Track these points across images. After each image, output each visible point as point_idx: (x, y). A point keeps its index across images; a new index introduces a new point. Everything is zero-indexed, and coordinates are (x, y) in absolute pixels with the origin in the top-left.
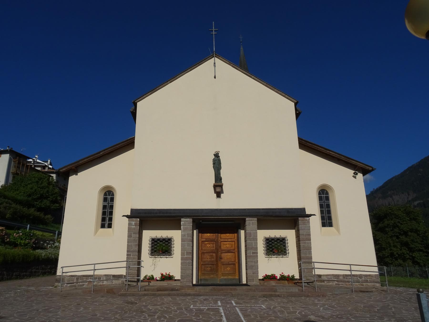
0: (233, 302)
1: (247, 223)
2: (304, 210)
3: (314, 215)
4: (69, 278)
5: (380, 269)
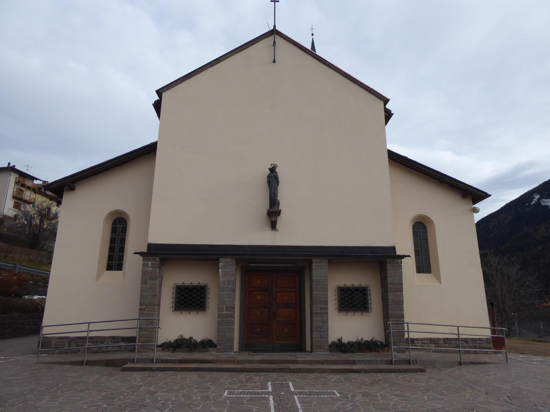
0: (291, 384)
1: (314, 266)
2: (393, 249)
3: (409, 256)
4: (58, 340)
5: (493, 332)
